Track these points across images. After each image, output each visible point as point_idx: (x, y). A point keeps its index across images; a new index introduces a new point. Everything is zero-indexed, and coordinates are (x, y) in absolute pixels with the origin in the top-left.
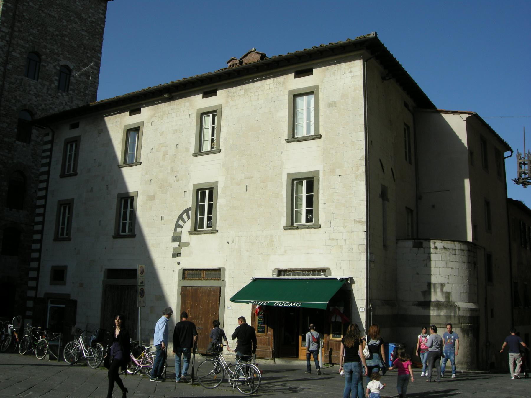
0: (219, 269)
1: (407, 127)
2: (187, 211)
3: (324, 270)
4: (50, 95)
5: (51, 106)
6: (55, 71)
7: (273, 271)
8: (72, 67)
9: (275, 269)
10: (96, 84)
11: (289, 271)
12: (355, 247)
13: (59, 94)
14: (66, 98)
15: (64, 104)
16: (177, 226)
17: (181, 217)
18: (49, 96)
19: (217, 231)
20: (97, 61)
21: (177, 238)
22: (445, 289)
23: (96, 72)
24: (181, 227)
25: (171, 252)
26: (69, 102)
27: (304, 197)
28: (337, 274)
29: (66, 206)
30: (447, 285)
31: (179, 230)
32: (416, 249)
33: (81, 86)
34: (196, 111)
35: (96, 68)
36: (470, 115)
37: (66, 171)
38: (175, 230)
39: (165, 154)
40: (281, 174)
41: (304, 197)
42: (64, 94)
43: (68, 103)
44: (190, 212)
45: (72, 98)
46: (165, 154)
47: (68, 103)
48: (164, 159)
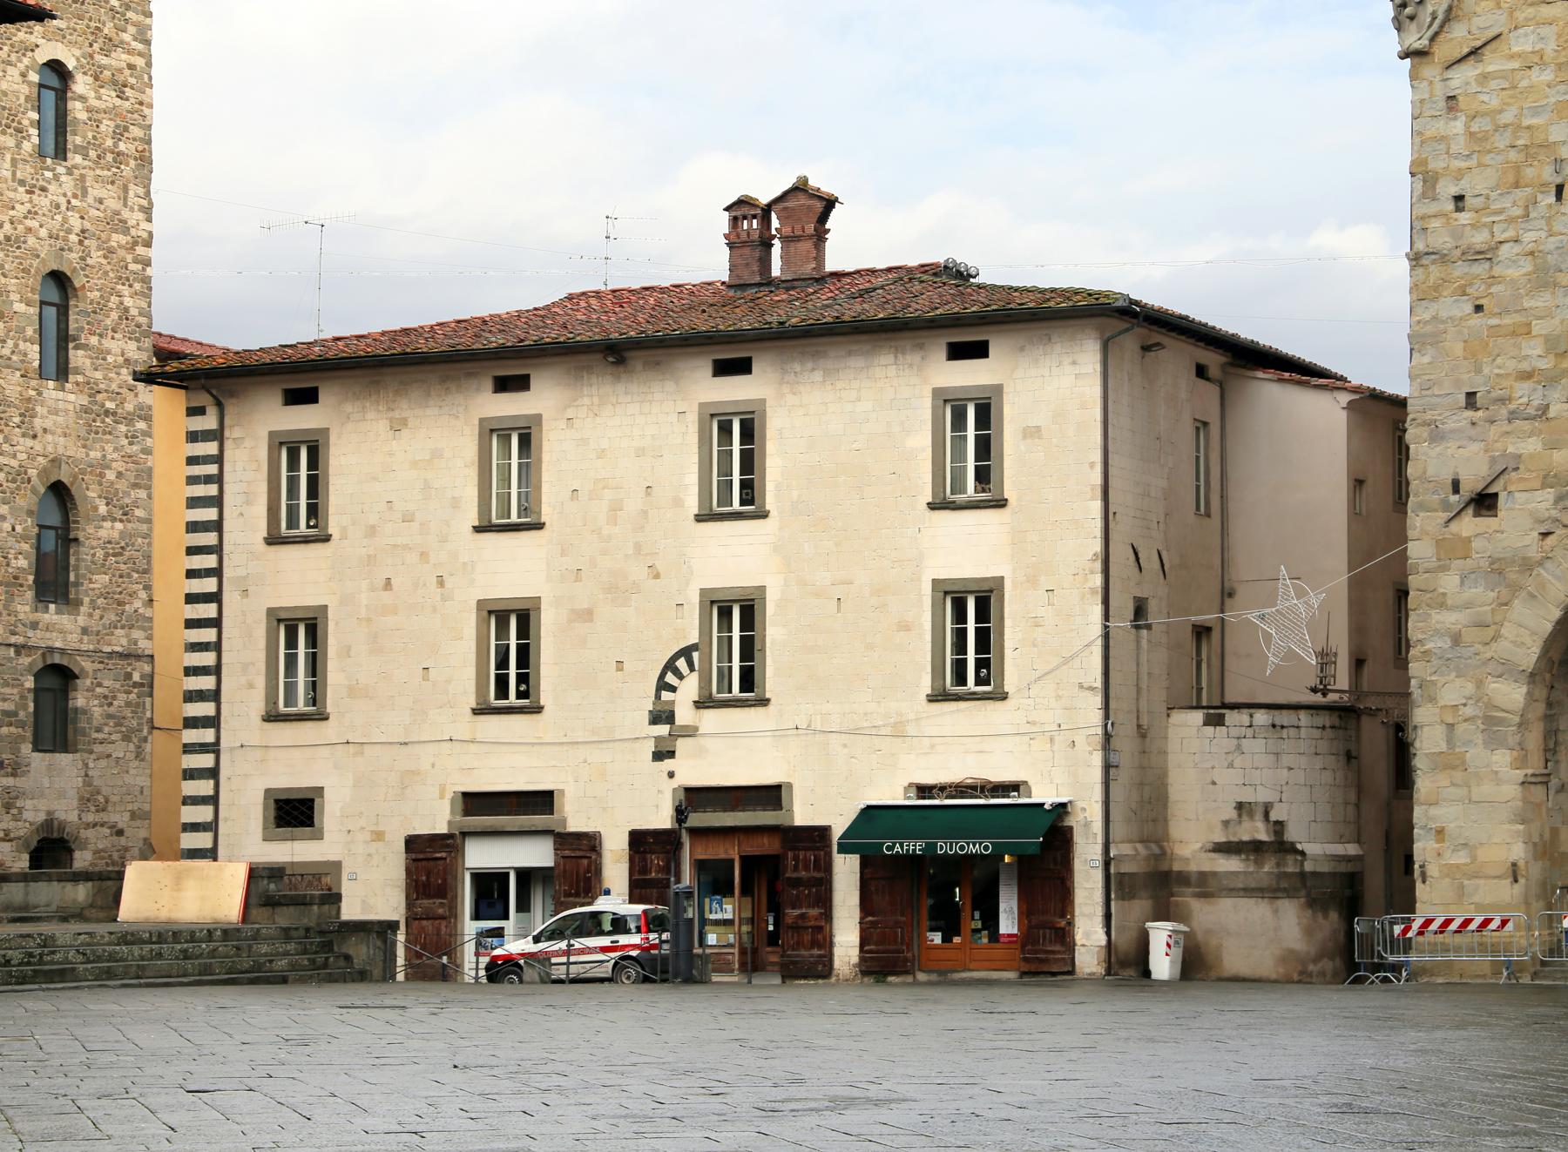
0: (777, 788)
1: (1202, 425)
2: (686, 652)
3: (1015, 787)
4: (22, 183)
5: (29, 223)
6: (25, 89)
7: (906, 789)
8: (71, 64)
9: (910, 785)
10: (146, 111)
11: (942, 788)
12: (1080, 739)
13: (49, 174)
14: (68, 183)
15: (63, 207)
16: (663, 686)
17: (670, 666)
18: (21, 189)
19: (768, 700)
20: (141, 18)
21: (662, 716)
22: (1273, 817)
23: (140, 62)
24: (673, 689)
25: (650, 747)
26: (75, 196)
27: (971, 637)
28: (1044, 794)
29: (302, 630)
30: (1277, 806)
31: (666, 695)
32: (1211, 729)
33: (103, 128)
34: (696, 408)
35: (140, 46)
36: (1357, 397)
37: (284, 525)
38: (658, 697)
39: (615, 508)
40: (919, 580)
41: (971, 637)
42: (60, 170)
43: (74, 202)
44: (695, 655)
45: (83, 178)
46: (615, 508)
47: (74, 202)
48: (613, 520)
